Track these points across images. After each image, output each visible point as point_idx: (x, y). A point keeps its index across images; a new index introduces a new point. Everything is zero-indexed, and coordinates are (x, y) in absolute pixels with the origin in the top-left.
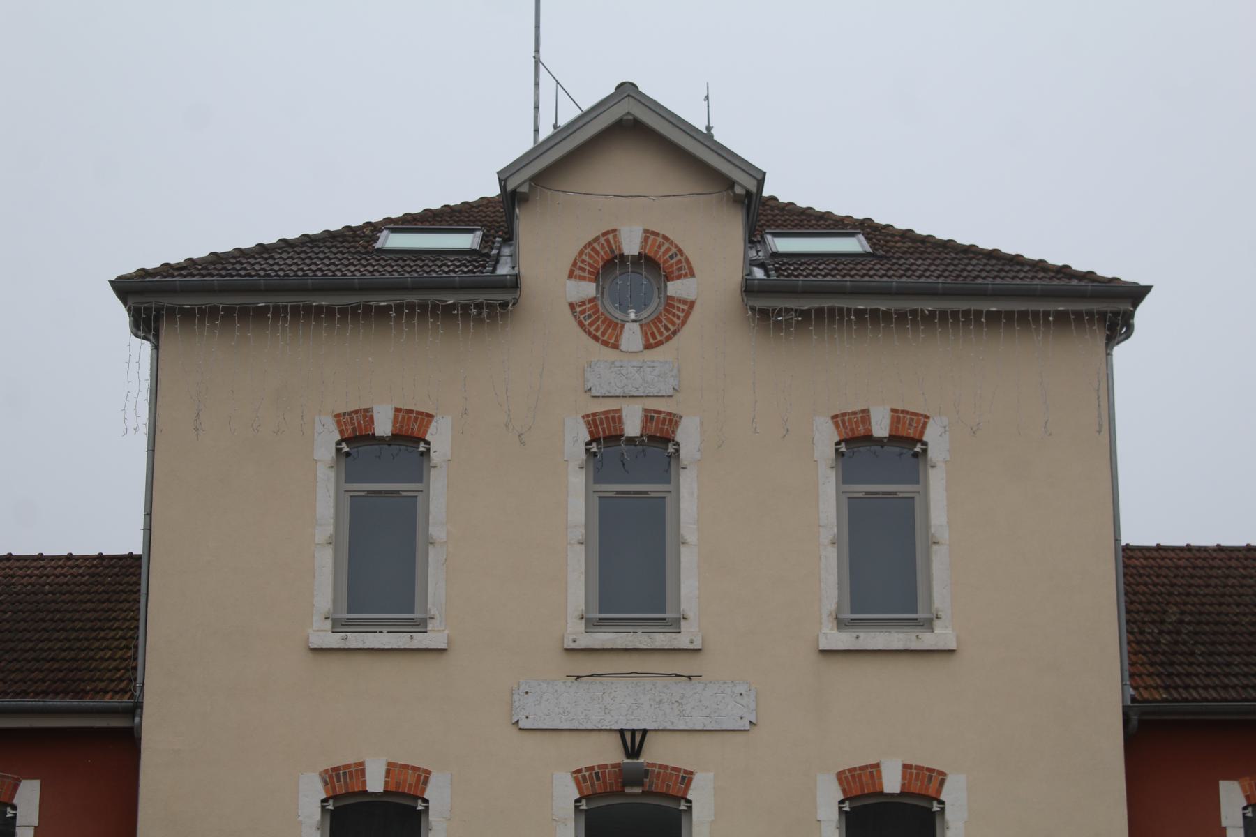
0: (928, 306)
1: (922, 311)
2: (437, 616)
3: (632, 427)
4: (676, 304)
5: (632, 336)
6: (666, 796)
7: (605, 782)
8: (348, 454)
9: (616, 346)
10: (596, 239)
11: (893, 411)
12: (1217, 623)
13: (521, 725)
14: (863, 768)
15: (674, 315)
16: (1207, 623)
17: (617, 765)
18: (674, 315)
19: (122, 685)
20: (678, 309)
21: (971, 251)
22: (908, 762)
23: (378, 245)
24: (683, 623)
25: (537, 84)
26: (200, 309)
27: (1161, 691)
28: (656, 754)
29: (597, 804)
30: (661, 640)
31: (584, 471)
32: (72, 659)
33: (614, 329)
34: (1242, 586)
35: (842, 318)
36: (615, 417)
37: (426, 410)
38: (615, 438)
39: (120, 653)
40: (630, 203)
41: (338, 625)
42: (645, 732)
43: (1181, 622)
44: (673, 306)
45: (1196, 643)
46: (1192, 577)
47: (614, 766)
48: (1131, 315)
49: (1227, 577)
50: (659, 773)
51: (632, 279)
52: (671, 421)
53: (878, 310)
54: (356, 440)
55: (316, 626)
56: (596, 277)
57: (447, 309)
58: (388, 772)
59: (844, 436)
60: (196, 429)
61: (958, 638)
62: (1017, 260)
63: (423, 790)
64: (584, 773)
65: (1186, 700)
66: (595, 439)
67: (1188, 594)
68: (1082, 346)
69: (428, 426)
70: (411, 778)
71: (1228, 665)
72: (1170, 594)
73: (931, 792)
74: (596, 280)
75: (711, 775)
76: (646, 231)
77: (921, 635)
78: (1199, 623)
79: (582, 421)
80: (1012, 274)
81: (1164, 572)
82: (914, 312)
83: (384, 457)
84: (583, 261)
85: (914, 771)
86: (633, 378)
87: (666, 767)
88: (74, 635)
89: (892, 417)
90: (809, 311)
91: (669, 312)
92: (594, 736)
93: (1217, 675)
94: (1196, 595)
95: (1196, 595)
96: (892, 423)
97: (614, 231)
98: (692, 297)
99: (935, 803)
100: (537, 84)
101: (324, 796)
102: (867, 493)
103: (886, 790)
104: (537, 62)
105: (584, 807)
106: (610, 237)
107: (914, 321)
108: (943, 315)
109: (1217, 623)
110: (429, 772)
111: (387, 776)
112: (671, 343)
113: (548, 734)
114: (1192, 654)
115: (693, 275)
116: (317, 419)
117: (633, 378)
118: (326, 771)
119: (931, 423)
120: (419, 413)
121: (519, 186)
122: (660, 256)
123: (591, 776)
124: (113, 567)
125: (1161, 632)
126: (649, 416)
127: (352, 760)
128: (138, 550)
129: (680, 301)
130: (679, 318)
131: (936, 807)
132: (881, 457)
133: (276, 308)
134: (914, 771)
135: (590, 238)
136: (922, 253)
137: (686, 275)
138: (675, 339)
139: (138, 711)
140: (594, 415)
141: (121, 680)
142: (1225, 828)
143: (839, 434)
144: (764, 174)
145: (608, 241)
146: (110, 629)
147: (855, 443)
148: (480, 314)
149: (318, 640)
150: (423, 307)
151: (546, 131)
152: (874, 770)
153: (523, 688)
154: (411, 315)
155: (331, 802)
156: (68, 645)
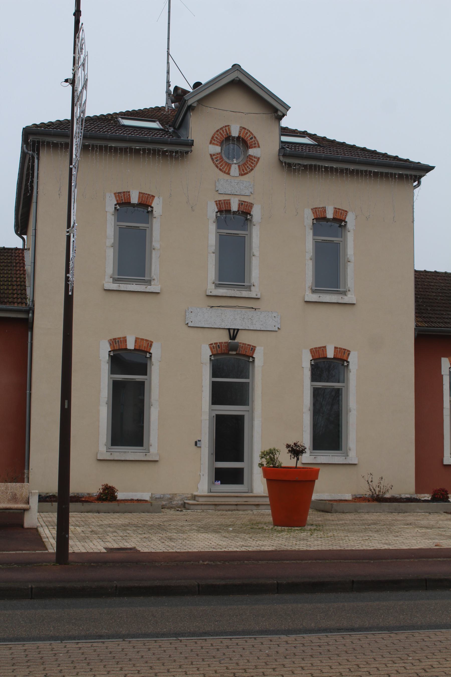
0: (352, 167)
1: (350, 169)
2: (156, 279)
3: (234, 207)
4: (253, 158)
5: (234, 170)
7: (222, 349)
9: (228, 174)
13: (189, 325)
22: (336, 346)
26: (61, 144)
28: (241, 339)
30: (245, 294)
36: (228, 203)
38: (229, 211)
44: (252, 160)
47: (225, 343)
48: (421, 177)
50: (242, 347)
51: (236, 146)
53: (333, 167)
54: (123, 203)
56: (221, 144)
57: (164, 152)
58: (136, 341)
60: (59, 194)
62: (375, 152)
64: (213, 345)
66: (220, 211)
73: (345, 358)
75: (262, 348)
77: (343, 297)
79: (311, 210)
82: (347, 169)
83: (134, 211)
85: (339, 350)
86: (235, 187)
87: (245, 344)
90: (307, 165)
92: (217, 330)
97: (228, 126)
98: (259, 156)
101: (110, 350)
103: (328, 357)
104: (168, 54)
105: (213, 359)
106: (227, 128)
107: (346, 173)
108: (357, 171)
110: (152, 342)
111: (136, 343)
113: (199, 329)
115: (259, 147)
117: (235, 187)
118: (111, 340)
121: (193, 103)
123: (216, 346)
126: (241, 203)
127: (121, 335)
129: (255, 157)
131: (148, 356)
132: (330, 225)
133: (93, 146)
134: (339, 350)
135: (219, 128)
138: (253, 172)
139: (31, 311)
140: (220, 201)
142: (443, 375)
143: (314, 216)
147: (320, 219)
149: (107, 287)
152: (324, 348)
154: (149, 153)
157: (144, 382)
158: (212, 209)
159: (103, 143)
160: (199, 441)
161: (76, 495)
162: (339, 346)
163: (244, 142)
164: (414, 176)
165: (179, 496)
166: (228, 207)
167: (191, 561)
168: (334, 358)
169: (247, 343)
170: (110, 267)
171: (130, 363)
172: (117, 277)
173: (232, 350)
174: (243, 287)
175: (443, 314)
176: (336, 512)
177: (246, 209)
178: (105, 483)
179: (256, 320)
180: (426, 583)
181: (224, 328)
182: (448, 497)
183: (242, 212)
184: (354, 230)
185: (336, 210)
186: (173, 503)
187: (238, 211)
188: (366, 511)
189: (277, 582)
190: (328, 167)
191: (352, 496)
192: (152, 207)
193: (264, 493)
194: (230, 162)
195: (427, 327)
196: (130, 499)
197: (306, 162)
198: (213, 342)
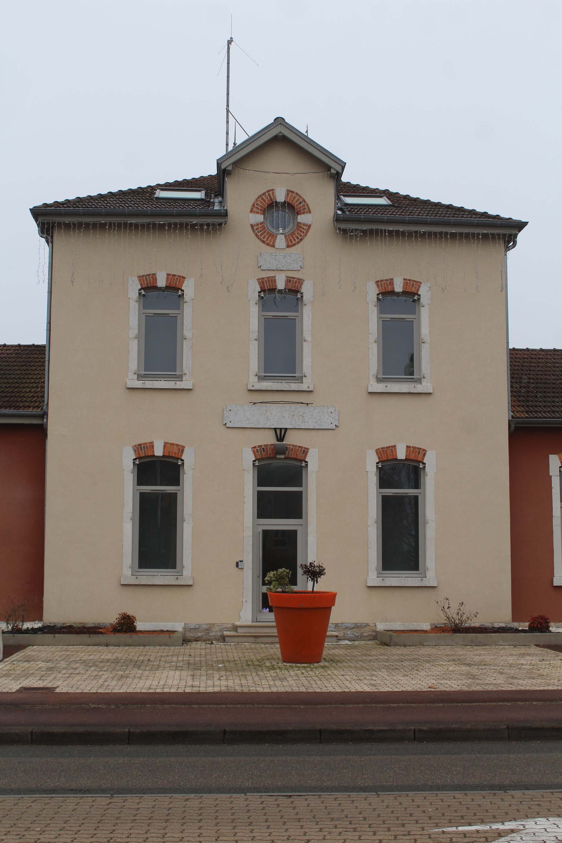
0: (423, 229)
1: (420, 231)
2: (188, 373)
3: (281, 285)
4: (302, 226)
5: (281, 241)
6: (296, 459)
8: (144, 296)
9: (273, 246)
10: (264, 194)
11: (404, 279)
12: (545, 383)
13: (228, 426)
14: (388, 447)
15: (301, 231)
16: (541, 383)
17: (273, 445)
18: (301, 231)
19: (37, 404)
20: (303, 229)
21: (438, 205)
23: (156, 196)
24: (304, 378)
25: (228, 122)
27: (525, 413)
28: (291, 440)
29: (263, 463)
30: (294, 386)
32: (11, 392)
33: (272, 237)
34: (554, 367)
35: (381, 235)
36: (272, 280)
37: (182, 275)
38: (273, 290)
39: (33, 390)
40: (281, 176)
41: (140, 377)
42: (286, 429)
43: (529, 382)
44: (301, 227)
45: (537, 392)
46: (531, 362)
47: (271, 445)
48: (516, 236)
49: (547, 363)
50: (292, 449)
51: (282, 212)
52: (299, 282)
54: (148, 288)
55: (130, 377)
56: (264, 212)
57: (193, 226)
58: (165, 446)
59: (381, 291)
60: (72, 282)
61: (433, 389)
62: (461, 209)
63: (181, 455)
65: (536, 418)
66: (263, 290)
67: (530, 370)
68: (491, 251)
69: (183, 282)
70: (175, 450)
71: (554, 402)
72: (522, 370)
73: (420, 459)
74: (264, 214)
76: (288, 190)
78: (537, 383)
79: (256, 281)
80: (460, 216)
81: (518, 360)
82: (416, 232)
83: (161, 295)
84: (257, 204)
85: (412, 449)
86: (281, 261)
87: (296, 446)
88: (11, 381)
89: (404, 282)
90: (366, 230)
91: (299, 230)
92: (263, 431)
93: (549, 406)
94: (534, 371)
95: (534, 371)
96: (404, 285)
97: (273, 190)
99: (421, 464)
100: (228, 122)
101: (135, 457)
102: (391, 318)
103: (398, 458)
104: (228, 111)
105: (257, 464)
106: (271, 193)
107: (416, 236)
108: (430, 234)
109: (545, 383)
110: (184, 447)
112: (299, 244)
113: (240, 430)
114: (536, 397)
115: (310, 212)
116: (130, 278)
117: (281, 261)
118: (135, 446)
119: (422, 285)
120: (179, 276)
121: (334, 169)
122: (295, 203)
123: (260, 449)
124: (26, 350)
125: (521, 387)
126: (289, 280)
127: (148, 441)
128: (41, 341)
129: (304, 225)
130: (303, 233)
131: (421, 466)
132: (398, 301)
133: (110, 224)
134: (412, 449)
136: (416, 205)
137: (307, 212)
138: (301, 243)
139: (46, 416)
140: (262, 278)
141: (36, 402)
143: (379, 290)
144: (345, 163)
145: (269, 195)
146: (28, 378)
147: (386, 294)
148: (208, 229)
149: (130, 385)
150: (181, 225)
151: (230, 148)
153: (229, 408)
155: (138, 460)
156: (8, 385)
157: (176, 494)
158: (254, 289)
160: (240, 561)
161: (96, 625)
162: (412, 445)
163: (292, 207)
165: (218, 626)
166: (273, 285)
167: (82, 704)
168: (406, 459)
171: (158, 471)
172: (381, 376)
173: (280, 454)
174: (294, 379)
175: (554, 402)
176: (396, 645)
177: (295, 286)
179: (309, 417)
180: (320, 734)
182: (549, 627)
183: (289, 290)
185: (406, 282)
186: (210, 634)
187: (285, 289)
189: (129, 731)
191: (431, 625)
193: (252, 622)
194: (274, 231)
195: (527, 418)
196: (158, 629)
197: (365, 227)
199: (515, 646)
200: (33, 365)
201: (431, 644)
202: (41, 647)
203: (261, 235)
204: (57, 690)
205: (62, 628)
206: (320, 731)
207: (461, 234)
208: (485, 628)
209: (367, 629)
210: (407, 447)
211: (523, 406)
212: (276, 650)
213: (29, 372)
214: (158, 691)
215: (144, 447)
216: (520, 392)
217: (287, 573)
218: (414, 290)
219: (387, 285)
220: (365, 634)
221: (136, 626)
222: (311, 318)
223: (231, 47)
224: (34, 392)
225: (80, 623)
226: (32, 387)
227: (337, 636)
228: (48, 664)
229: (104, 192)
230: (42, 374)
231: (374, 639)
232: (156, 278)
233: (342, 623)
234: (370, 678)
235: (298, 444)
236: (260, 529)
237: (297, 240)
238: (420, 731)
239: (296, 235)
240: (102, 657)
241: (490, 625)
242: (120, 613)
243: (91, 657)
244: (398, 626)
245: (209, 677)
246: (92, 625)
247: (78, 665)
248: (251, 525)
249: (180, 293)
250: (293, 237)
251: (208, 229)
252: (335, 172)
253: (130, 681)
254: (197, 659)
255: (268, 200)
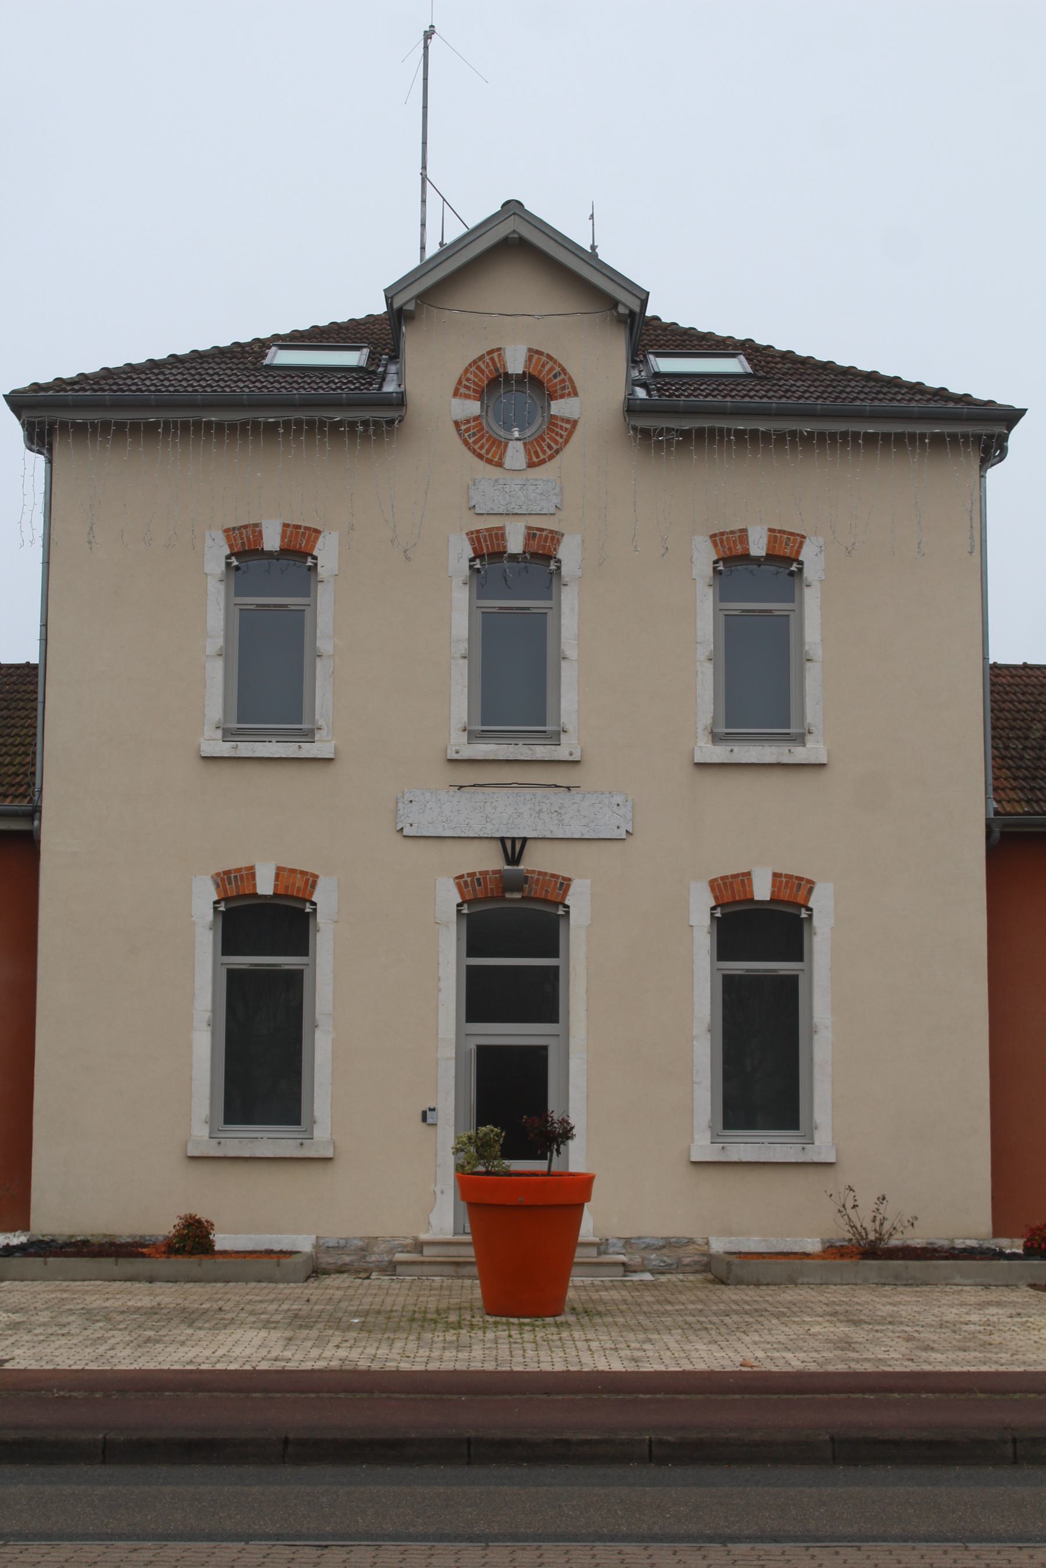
1: (801, 431)
2: (324, 726)
3: (515, 544)
4: (560, 423)
5: (515, 455)
7: (486, 887)
8: (237, 568)
9: (500, 465)
10: (481, 358)
11: (770, 530)
13: (406, 832)
14: (734, 876)
15: (557, 434)
17: (499, 872)
18: (557, 434)
19: (22, 790)
20: (561, 428)
23: (266, 362)
24: (563, 736)
25: (424, 201)
27: (1023, 804)
28: (534, 861)
30: (541, 752)
31: (468, 586)
33: (498, 447)
36: (498, 535)
38: (498, 555)
39: (18, 759)
40: (517, 322)
41: (228, 735)
42: (525, 840)
44: (556, 425)
47: (495, 872)
48: (1005, 438)
50: (538, 880)
51: (517, 398)
52: (553, 538)
53: (758, 430)
56: (479, 396)
57: (335, 426)
59: (722, 555)
60: (90, 542)
63: (311, 894)
64: (466, 878)
66: (478, 555)
68: (962, 465)
70: (299, 883)
72: (1035, 711)
73: (800, 900)
74: (480, 399)
75: (588, 882)
76: (530, 350)
77: (793, 749)
79: (466, 538)
80: (890, 396)
81: (1030, 689)
82: (793, 433)
83: (272, 571)
84: (468, 380)
85: (784, 880)
86: (516, 495)
87: (545, 874)
89: (770, 537)
90: (690, 431)
91: (552, 431)
92: (476, 842)
96: (769, 542)
97: (499, 349)
98: (575, 416)
100: (424, 201)
101: (216, 898)
102: (743, 611)
103: (756, 898)
104: (424, 178)
105: (465, 911)
106: (495, 355)
108: (821, 436)
110: (317, 877)
112: (554, 461)
113: (431, 842)
115: (576, 394)
117: (516, 495)
118: (218, 874)
119: (807, 542)
120: (306, 528)
121: (406, 303)
122: (544, 375)
123: (472, 881)
124: (11, 675)
125: (1025, 748)
126: (531, 534)
128: (35, 660)
129: (563, 420)
131: (804, 914)
132: (758, 577)
133: (167, 423)
134: (784, 880)
136: (802, 374)
137: (569, 395)
138: (558, 457)
139: (38, 815)
140: (478, 531)
141: (20, 784)
143: (717, 552)
144: (648, 293)
145: (492, 359)
148: (366, 431)
151: (432, 249)
155: (223, 904)
157: (301, 972)
158: (460, 553)
159: (190, 415)
160: (430, 1110)
161: (137, 1239)
163: (541, 383)
164: (973, 436)
165: (384, 1242)
166: (498, 545)
169: (550, 871)
170: (460, 706)
171: (264, 925)
173: (513, 890)
176: (740, 1282)
178: (183, 1212)
179: (572, 814)
180: (469, 1448)
181: (492, 838)
184: (821, 581)
186: (368, 1259)
187: (524, 552)
188: (818, 1281)
189: (105, 1438)
190: (744, 431)
191: (823, 1242)
192: (315, 558)
193: (455, 1234)
196: (263, 1248)
197: (687, 424)
198: (465, 872)
199: (987, 1286)
200: (23, 708)
201: (811, 1281)
202: (17, 1283)
203: (475, 442)
204: (8, 1366)
205: (67, 1244)
206: (469, 1441)
207: (886, 436)
208: (935, 1250)
209: (691, 1248)
210: (776, 875)
211: (1022, 789)
212: (472, 1290)
213: (13, 722)
214: (204, 1367)
215: (235, 877)
216: (1022, 758)
217: (497, 1135)
218: (788, 552)
219: (734, 542)
220: (686, 1261)
221: (213, 1241)
222: (576, 612)
223: (432, 44)
224: (19, 763)
225: (105, 1236)
226: (16, 753)
227: (624, 1264)
228: (13, 1316)
229: (160, 355)
230: (30, 726)
231: (704, 1271)
232: (260, 532)
233: (639, 1238)
234: (638, 1346)
235: (550, 870)
236: (472, 1044)
237: (549, 452)
238: (661, 1443)
239: (548, 440)
240: (130, 1303)
241: (945, 1243)
242: (182, 1214)
243: (107, 1304)
244: (753, 1244)
245: (321, 1341)
246: (129, 1240)
247: (72, 1318)
248: (452, 1036)
249: (310, 562)
250: (540, 446)
251: (366, 431)
252: (627, 312)
253: (160, 1350)
254: (317, 1307)
255: (490, 371)
